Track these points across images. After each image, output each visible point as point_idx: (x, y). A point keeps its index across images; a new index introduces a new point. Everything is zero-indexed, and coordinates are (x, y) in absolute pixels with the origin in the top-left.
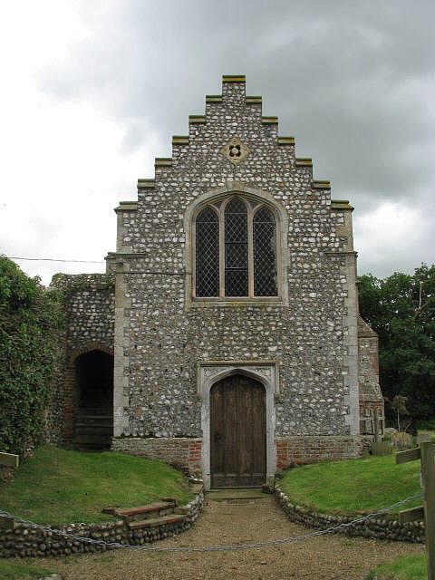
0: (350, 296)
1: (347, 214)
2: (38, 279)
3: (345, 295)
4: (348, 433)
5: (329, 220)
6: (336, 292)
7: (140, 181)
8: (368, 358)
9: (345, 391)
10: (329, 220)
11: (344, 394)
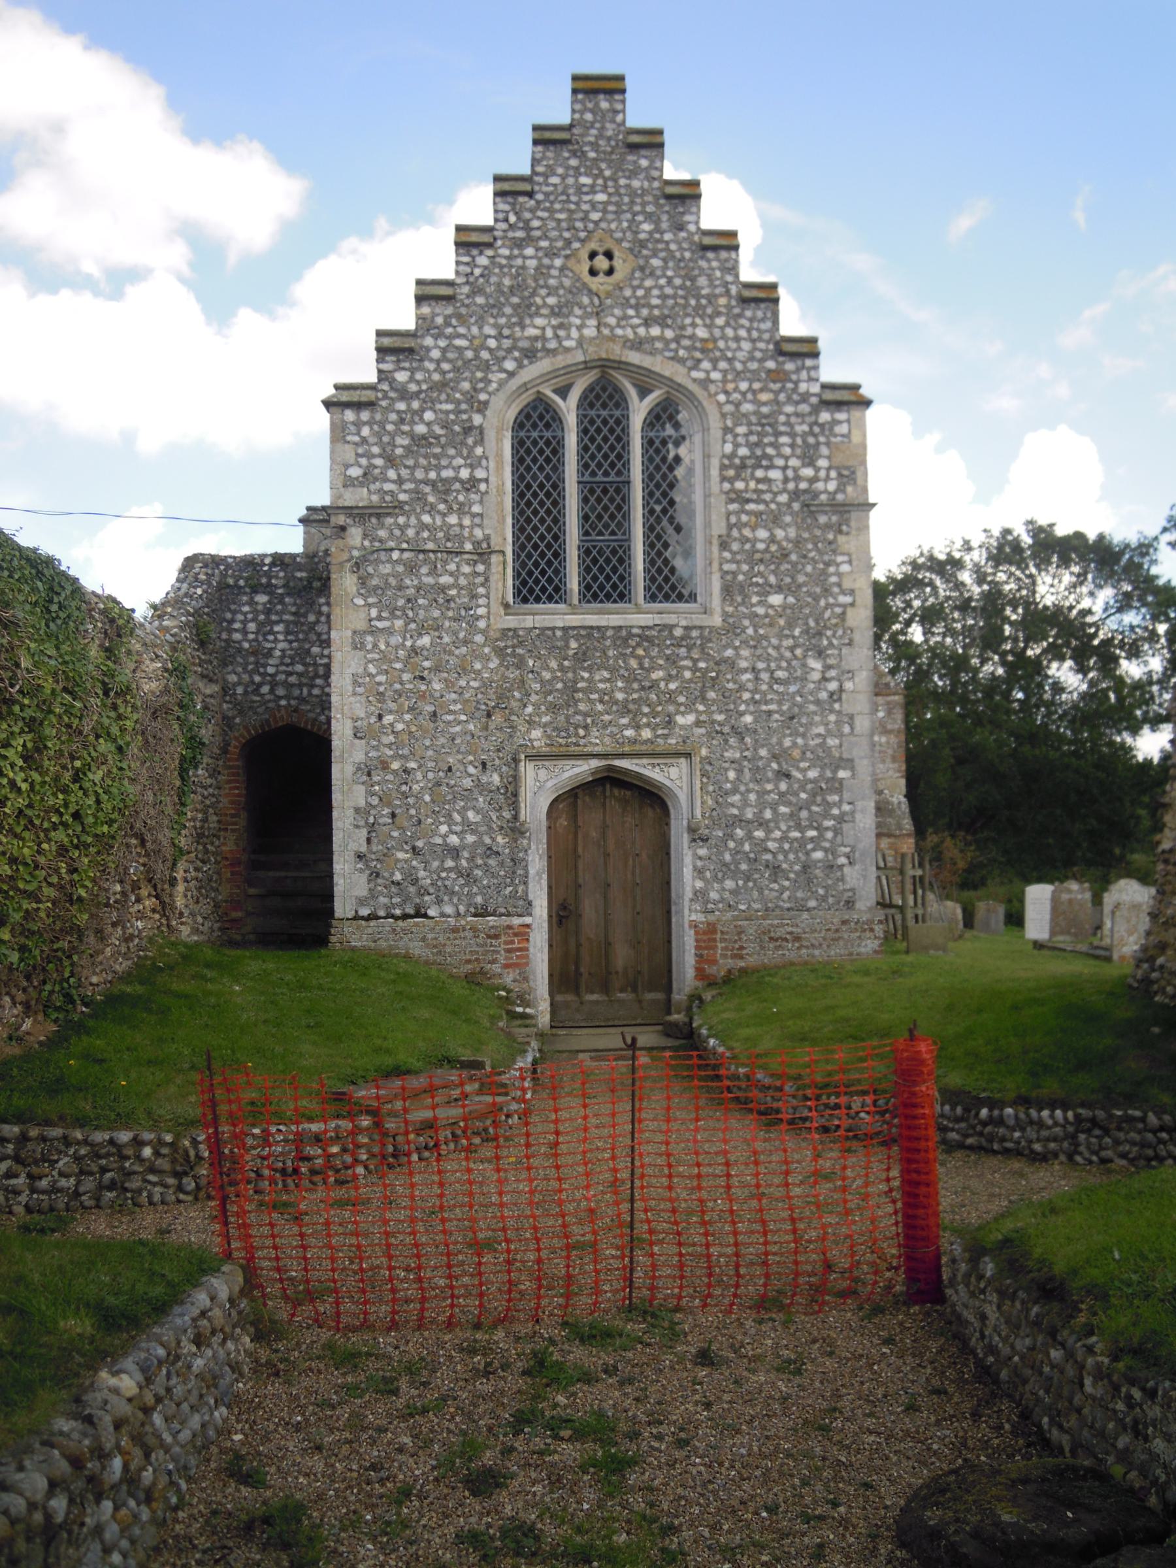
0: (859, 601)
1: (856, 413)
3: (848, 599)
4: (850, 904)
5: (816, 429)
6: (827, 591)
8: (884, 739)
9: (843, 814)
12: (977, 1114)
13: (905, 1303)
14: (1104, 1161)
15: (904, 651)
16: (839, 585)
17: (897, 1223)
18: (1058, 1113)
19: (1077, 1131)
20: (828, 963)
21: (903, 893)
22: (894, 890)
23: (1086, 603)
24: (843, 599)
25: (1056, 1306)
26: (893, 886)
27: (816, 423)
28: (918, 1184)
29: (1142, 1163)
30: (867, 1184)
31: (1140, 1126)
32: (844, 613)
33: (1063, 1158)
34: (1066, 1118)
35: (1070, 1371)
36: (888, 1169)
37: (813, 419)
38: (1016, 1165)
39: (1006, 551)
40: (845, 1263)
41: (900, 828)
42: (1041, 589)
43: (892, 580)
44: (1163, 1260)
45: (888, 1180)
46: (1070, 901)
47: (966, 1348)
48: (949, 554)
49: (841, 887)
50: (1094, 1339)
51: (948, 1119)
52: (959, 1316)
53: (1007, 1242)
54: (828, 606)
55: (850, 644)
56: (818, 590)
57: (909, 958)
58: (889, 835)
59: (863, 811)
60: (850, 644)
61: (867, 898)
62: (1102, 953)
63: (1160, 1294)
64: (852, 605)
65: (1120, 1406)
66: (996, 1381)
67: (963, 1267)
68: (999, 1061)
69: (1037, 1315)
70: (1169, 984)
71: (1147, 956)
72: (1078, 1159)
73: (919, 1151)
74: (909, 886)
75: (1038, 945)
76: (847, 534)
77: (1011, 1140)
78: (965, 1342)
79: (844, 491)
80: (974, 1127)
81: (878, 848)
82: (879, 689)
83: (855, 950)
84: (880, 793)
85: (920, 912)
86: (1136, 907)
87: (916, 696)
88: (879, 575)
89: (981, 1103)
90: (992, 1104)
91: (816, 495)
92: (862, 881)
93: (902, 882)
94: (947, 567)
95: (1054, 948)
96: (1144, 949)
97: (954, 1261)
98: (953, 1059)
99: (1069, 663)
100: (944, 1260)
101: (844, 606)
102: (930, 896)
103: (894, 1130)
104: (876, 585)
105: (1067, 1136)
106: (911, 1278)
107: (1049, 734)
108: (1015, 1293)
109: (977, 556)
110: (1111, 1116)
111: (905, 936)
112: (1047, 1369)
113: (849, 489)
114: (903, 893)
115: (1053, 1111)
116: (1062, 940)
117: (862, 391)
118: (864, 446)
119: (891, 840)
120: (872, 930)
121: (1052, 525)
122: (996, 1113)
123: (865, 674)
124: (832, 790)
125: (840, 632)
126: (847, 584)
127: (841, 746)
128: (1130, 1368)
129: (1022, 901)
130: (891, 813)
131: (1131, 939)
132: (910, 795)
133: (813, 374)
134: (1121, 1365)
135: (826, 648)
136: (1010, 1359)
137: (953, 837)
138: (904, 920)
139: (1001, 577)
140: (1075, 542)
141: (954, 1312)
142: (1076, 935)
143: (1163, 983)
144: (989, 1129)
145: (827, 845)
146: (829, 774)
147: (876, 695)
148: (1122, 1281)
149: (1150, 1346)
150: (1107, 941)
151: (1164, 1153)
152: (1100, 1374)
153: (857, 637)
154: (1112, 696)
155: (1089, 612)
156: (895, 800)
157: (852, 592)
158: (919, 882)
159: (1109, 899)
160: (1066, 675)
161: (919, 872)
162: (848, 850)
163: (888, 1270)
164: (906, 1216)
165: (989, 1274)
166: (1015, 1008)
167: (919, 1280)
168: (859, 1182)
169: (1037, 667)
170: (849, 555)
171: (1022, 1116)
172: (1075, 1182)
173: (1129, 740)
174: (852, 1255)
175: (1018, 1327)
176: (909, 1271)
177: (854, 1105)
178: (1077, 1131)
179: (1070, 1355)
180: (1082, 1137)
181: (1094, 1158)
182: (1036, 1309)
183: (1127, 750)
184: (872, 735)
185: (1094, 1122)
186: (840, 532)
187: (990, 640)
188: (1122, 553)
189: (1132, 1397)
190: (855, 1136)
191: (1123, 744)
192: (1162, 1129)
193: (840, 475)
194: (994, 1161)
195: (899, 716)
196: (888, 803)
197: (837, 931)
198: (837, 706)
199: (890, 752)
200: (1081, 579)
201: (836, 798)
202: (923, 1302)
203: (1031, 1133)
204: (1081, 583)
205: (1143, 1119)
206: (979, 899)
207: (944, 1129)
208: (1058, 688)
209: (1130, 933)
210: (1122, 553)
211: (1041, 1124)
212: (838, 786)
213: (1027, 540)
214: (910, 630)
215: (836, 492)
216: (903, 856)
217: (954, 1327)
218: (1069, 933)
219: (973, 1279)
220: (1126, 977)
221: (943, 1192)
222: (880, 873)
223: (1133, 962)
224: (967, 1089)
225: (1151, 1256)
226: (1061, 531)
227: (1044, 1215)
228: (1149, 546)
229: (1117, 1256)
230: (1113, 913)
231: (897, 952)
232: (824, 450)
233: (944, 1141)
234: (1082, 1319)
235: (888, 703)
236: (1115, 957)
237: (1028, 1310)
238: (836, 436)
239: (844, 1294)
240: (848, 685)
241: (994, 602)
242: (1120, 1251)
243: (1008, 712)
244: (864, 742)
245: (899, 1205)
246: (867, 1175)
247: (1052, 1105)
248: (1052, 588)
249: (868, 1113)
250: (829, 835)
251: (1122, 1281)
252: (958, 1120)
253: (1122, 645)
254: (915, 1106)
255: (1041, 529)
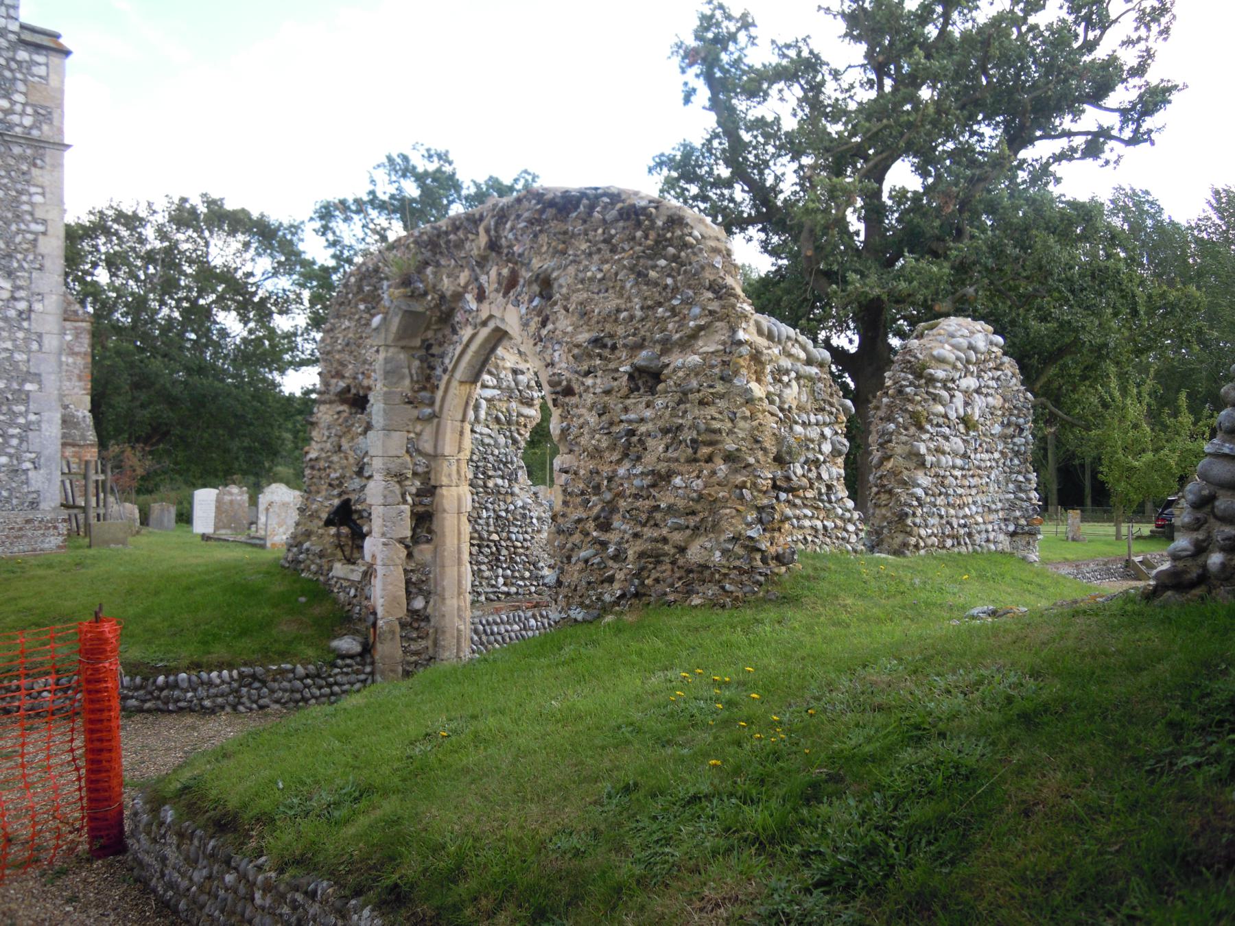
0: (51, 231)
1: (55, 60)
2: (320, 374)
3: (40, 228)
4: (34, 505)
5: (14, 65)
6: (18, 217)
7: (491, 178)
8: (70, 360)
9: (29, 423)
10: (14, 65)
11: (27, 428)
12: (155, 681)
13: (88, 860)
14: (261, 707)
15: (92, 291)
16: (32, 214)
17: (80, 789)
18: (225, 672)
19: (241, 686)
20: (11, 559)
21: (86, 495)
22: (77, 494)
23: (248, 268)
24: (34, 227)
25: (230, 837)
26: (76, 489)
27: (13, 59)
28: (101, 750)
29: (291, 705)
30: (48, 757)
31: (291, 675)
32: (35, 240)
33: (228, 709)
34: (231, 677)
35: (242, 890)
36: (72, 740)
37: (10, 54)
38: (189, 720)
39: (184, 217)
40: (25, 833)
41: (84, 438)
42: (213, 250)
43: (82, 227)
44: (317, 782)
45: (72, 750)
46: (231, 502)
47: (146, 888)
48: (134, 212)
49: (25, 489)
50: (263, 859)
51: (128, 688)
52: (140, 863)
53: (186, 789)
54: (19, 231)
55: (41, 269)
56: (10, 215)
57: (92, 552)
58: (74, 445)
59: (49, 421)
60: (41, 269)
61: (51, 498)
62: (258, 542)
63: (317, 811)
64: (44, 233)
65: (286, 910)
66: (176, 912)
67: (145, 818)
68: (175, 635)
69: (214, 848)
70: (313, 563)
71: (295, 543)
72: (241, 708)
73: (102, 721)
74: (92, 489)
75: (206, 538)
76: (41, 168)
77: (185, 700)
78: (146, 883)
79: (40, 129)
80: (151, 693)
81: (63, 457)
82: (68, 316)
83: (39, 546)
84: (66, 407)
85: (102, 512)
86: (285, 505)
87: (101, 329)
88: (70, 219)
89: (158, 671)
90: (168, 671)
91: (11, 126)
92: (47, 484)
93: (86, 486)
94: (132, 221)
95: (219, 539)
96: (294, 536)
97: (136, 814)
98: (132, 636)
99: (234, 313)
100: (126, 813)
101: (36, 234)
102: (111, 499)
103: (77, 704)
104: (68, 226)
105: (232, 691)
106: (94, 835)
107: (214, 366)
108: (193, 832)
109: (161, 218)
110: (268, 671)
111: (88, 532)
112: (222, 892)
113: (45, 127)
114: (86, 495)
115: (220, 672)
116: (223, 533)
117: (61, 41)
118: (62, 91)
119: (76, 449)
120: (55, 528)
121: (221, 200)
122: (172, 678)
123: (54, 297)
124: (17, 401)
125: (31, 257)
126: (39, 214)
127: (29, 361)
128: (294, 877)
129: (191, 504)
130: (76, 425)
131: (281, 530)
132: (95, 409)
133: (12, 12)
134: (286, 876)
135: (16, 270)
136: (188, 890)
137: (133, 448)
138: (86, 518)
139: (181, 237)
140: (241, 216)
141: (135, 859)
142: (235, 529)
143: (308, 562)
144: (165, 693)
145: (12, 451)
146: (15, 386)
147: (65, 320)
148: (285, 806)
149: (310, 855)
150: (262, 533)
151: (308, 695)
152: (267, 888)
153: (48, 264)
154: (267, 343)
155: (251, 274)
156: (80, 414)
157: (44, 222)
158: (101, 487)
159: (263, 499)
160: (230, 322)
161: (102, 477)
162: (33, 455)
163: (71, 832)
164: (90, 781)
165: (169, 820)
166: (189, 589)
167: (102, 837)
168: (41, 756)
169: (207, 313)
170: (42, 187)
171: (194, 678)
172: (238, 728)
173: (276, 376)
174: (35, 824)
175: (196, 861)
176: (91, 830)
177: (36, 687)
178: (241, 686)
179: (243, 877)
180: (244, 690)
181: (254, 706)
182: (212, 843)
183: (274, 385)
184: (60, 354)
185: (254, 677)
186: (35, 165)
187: (168, 286)
188: (278, 229)
189: (295, 900)
190: (38, 715)
191: (273, 381)
192: (307, 676)
193: (37, 113)
194: (168, 720)
195: (86, 340)
196: (73, 416)
197: (21, 529)
198: (25, 324)
199: (77, 371)
200: (247, 245)
201: (23, 408)
202: (106, 856)
203: (201, 692)
204: (246, 251)
205: (293, 671)
206: (155, 501)
207: (125, 698)
208: (224, 333)
209: (280, 526)
210: (278, 229)
211: (210, 684)
212: (26, 398)
213: (202, 209)
214: (96, 272)
215: (31, 128)
216: (87, 463)
217: (136, 872)
218: (230, 527)
219: (154, 827)
220: (279, 559)
221: (124, 753)
222: (64, 478)
223: (284, 549)
224: (146, 660)
225: (308, 781)
226: (230, 206)
227: (217, 760)
228: (297, 227)
229: (281, 786)
230: (267, 509)
231: (80, 547)
232: (21, 87)
233: (124, 709)
234: (253, 844)
235: (76, 328)
236: (268, 545)
237: (205, 845)
238: (33, 76)
239: (25, 864)
240: (38, 306)
241: (169, 258)
242: (284, 781)
243: (181, 348)
244: (53, 359)
245: (83, 771)
246: (48, 748)
247: (220, 667)
248: (222, 251)
249: (50, 691)
250: (15, 442)
251: (285, 806)
252: (137, 689)
253: (276, 304)
254: (99, 681)
255: (214, 202)
